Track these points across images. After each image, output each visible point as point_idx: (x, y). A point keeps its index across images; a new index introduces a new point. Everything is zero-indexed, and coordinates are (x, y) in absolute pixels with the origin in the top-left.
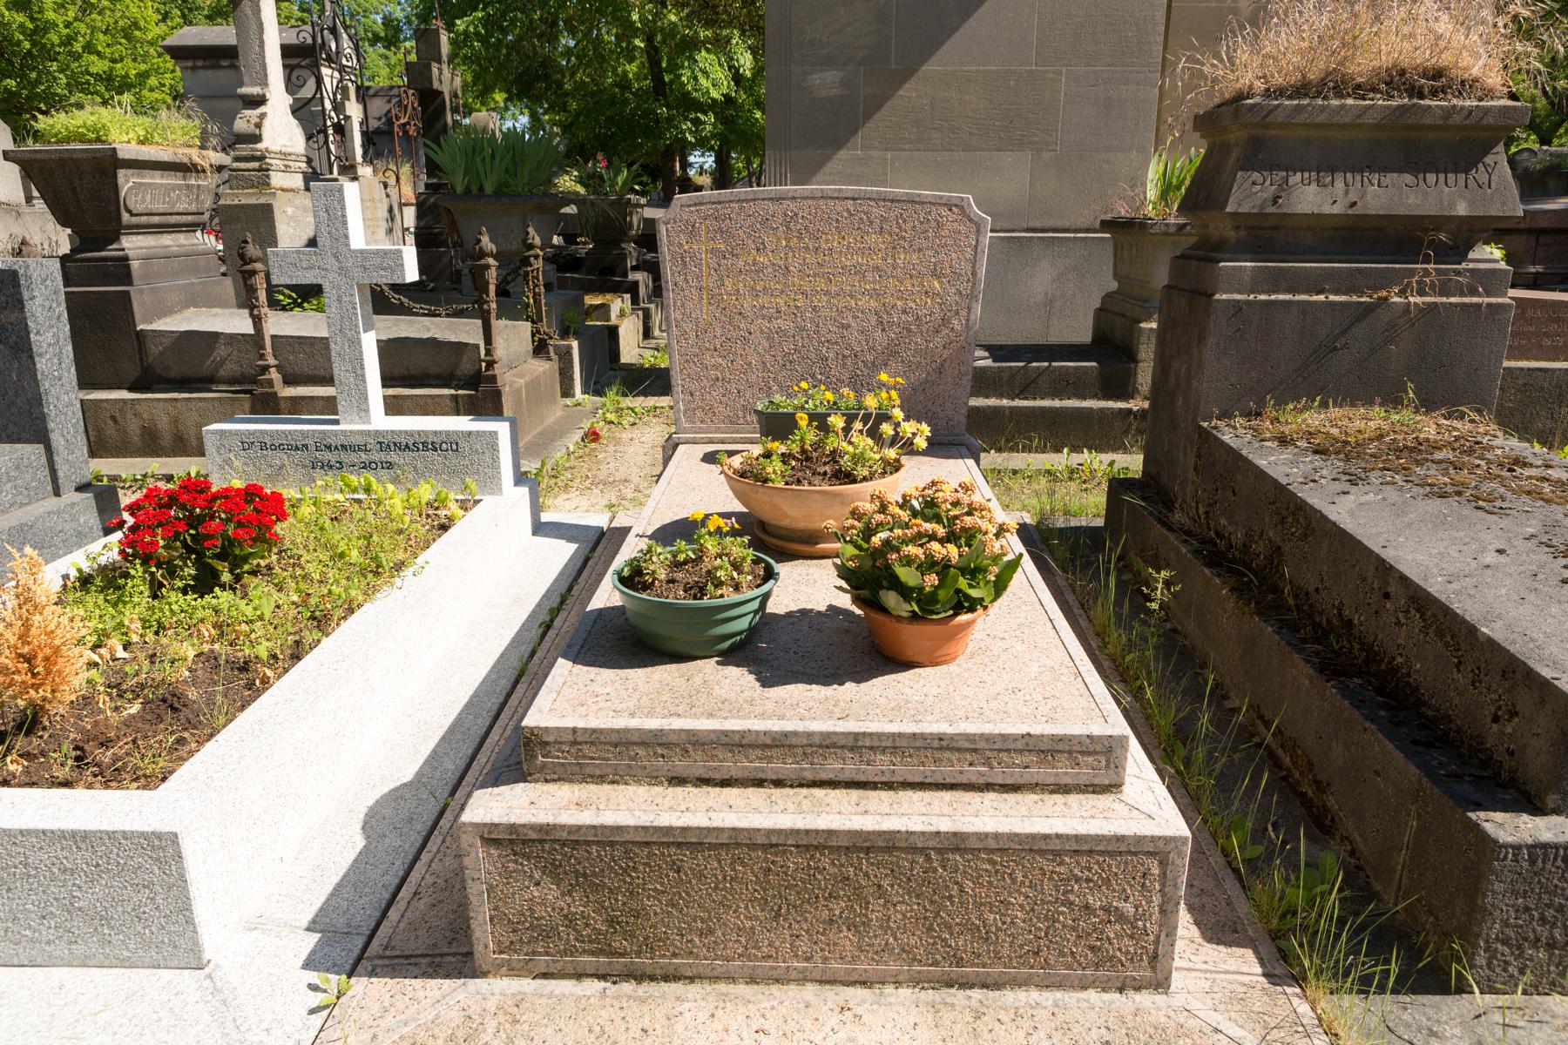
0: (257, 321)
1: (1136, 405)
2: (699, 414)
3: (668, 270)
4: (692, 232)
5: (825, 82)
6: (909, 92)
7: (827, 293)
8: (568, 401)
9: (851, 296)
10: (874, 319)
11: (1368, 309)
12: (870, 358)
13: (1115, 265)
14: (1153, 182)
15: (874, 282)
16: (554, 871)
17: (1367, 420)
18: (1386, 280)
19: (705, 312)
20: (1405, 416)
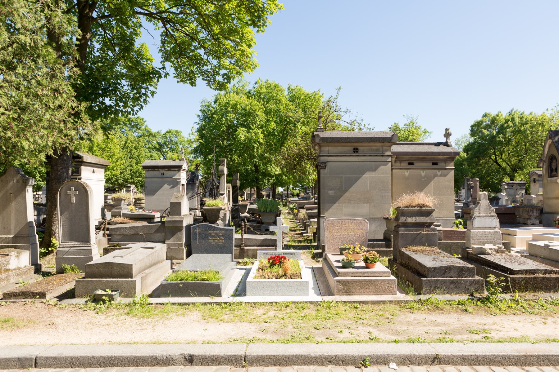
0: (242, 236)
1: (392, 249)
4: (328, 224)
5: (331, 192)
6: (346, 194)
11: (419, 234)
14: (391, 214)
16: (342, 284)
17: (421, 248)
18: (420, 230)
19: (330, 235)
20: (426, 247)
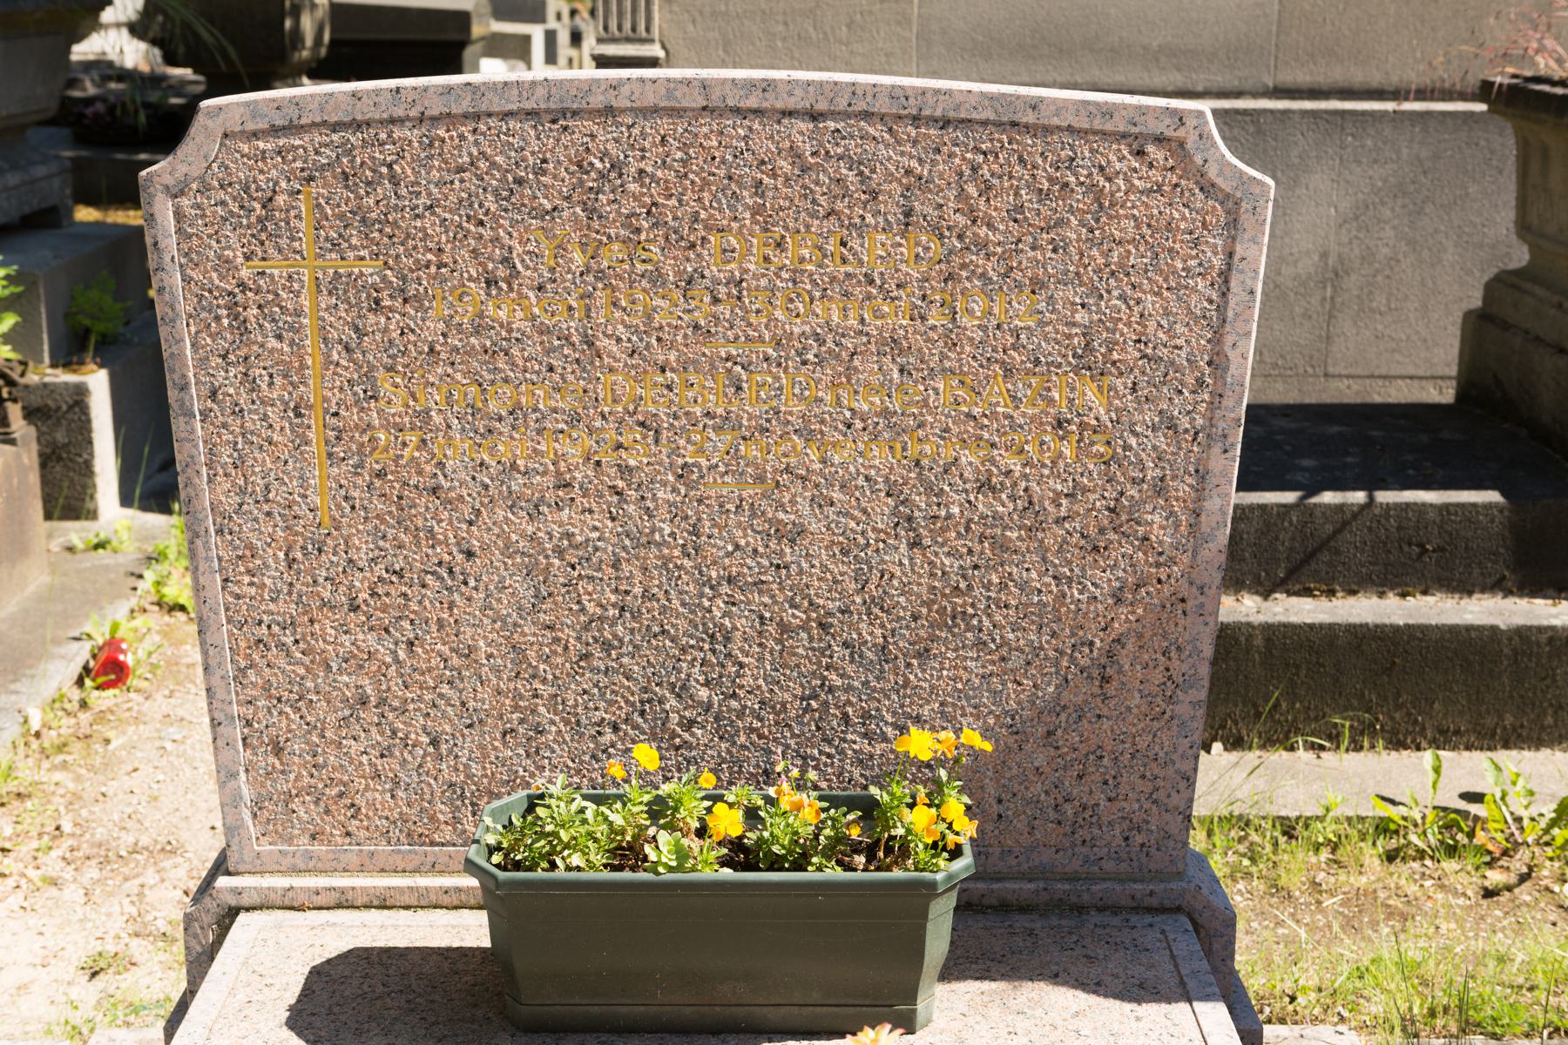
2: (304, 810)
3: (187, 347)
4: (266, 220)
7: (726, 423)
8: (75, 532)
9: (808, 435)
10: (882, 511)
12: (871, 634)
13: (1522, 203)
15: (886, 389)
19: (317, 485)
